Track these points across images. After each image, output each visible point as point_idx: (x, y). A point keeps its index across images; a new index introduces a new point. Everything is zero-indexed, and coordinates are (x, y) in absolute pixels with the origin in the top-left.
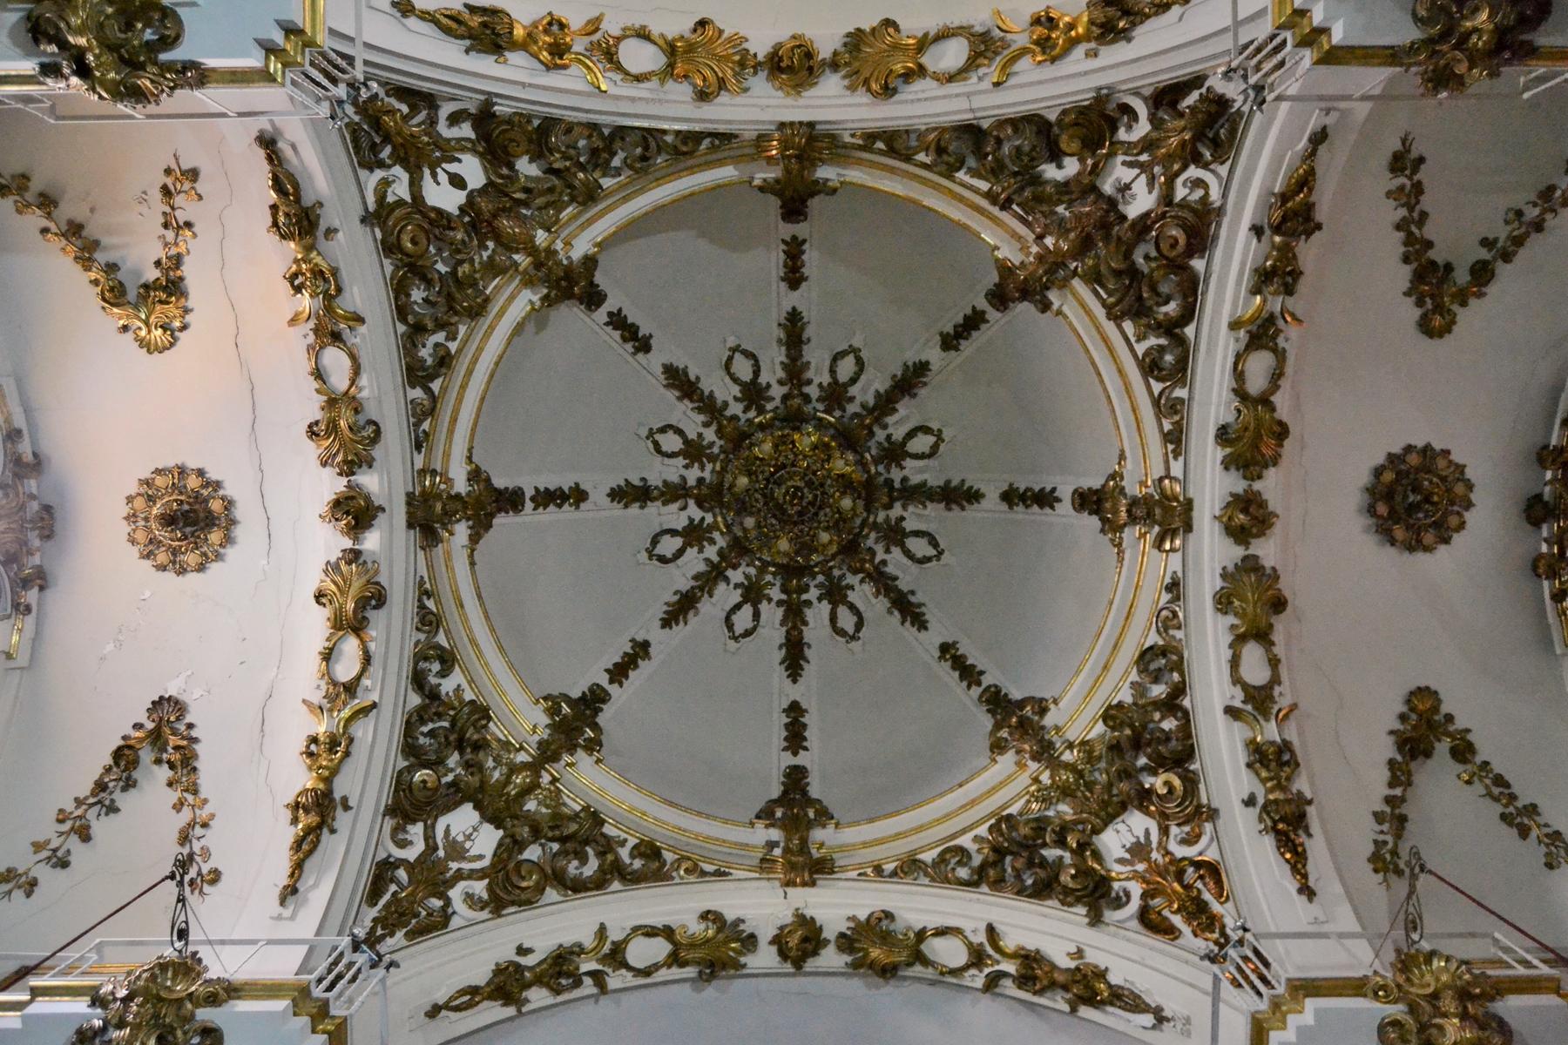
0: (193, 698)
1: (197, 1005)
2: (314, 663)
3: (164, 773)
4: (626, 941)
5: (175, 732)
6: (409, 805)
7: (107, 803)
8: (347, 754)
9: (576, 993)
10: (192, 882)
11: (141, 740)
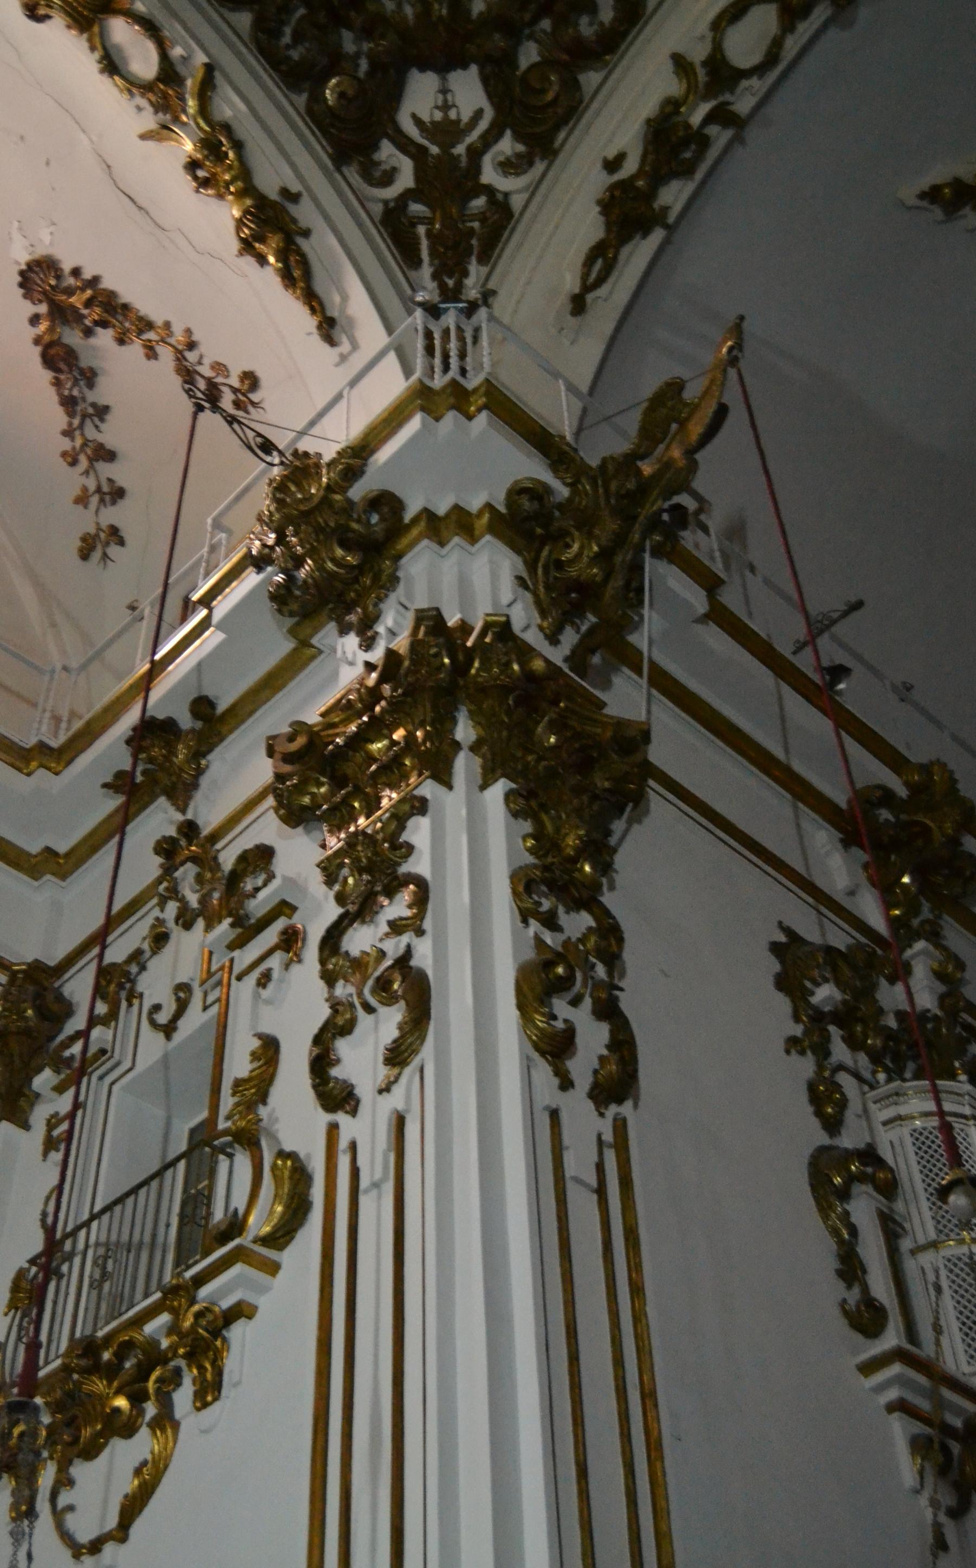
0: (46, 242)
1: (344, 490)
2: (107, 91)
3: (105, 337)
4: (718, 47)
5: (70, 292)
6: (351, 136)
7: (91, 410)
8: (238, 146)
9: (713, 154)
10: (237, 404)
11: (51, 330)
